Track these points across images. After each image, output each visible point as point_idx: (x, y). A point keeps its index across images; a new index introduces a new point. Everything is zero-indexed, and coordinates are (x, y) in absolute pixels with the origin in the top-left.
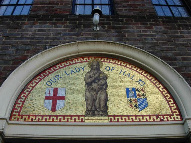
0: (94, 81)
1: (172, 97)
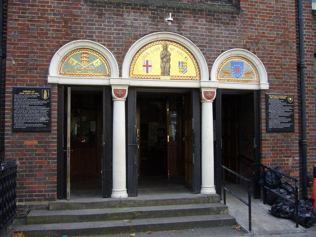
0: (164, 57)
1: (198, 68)
